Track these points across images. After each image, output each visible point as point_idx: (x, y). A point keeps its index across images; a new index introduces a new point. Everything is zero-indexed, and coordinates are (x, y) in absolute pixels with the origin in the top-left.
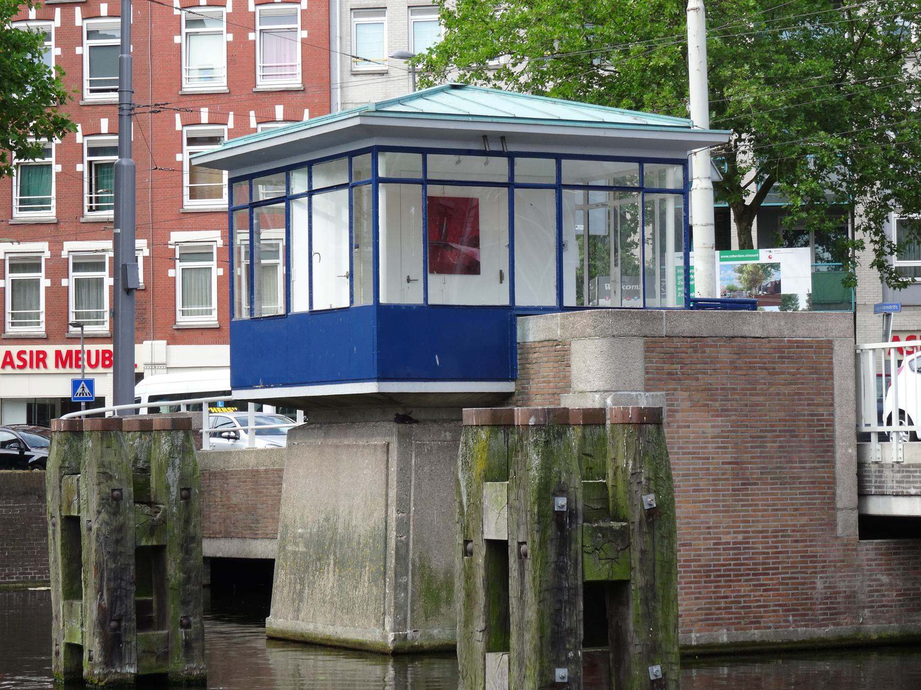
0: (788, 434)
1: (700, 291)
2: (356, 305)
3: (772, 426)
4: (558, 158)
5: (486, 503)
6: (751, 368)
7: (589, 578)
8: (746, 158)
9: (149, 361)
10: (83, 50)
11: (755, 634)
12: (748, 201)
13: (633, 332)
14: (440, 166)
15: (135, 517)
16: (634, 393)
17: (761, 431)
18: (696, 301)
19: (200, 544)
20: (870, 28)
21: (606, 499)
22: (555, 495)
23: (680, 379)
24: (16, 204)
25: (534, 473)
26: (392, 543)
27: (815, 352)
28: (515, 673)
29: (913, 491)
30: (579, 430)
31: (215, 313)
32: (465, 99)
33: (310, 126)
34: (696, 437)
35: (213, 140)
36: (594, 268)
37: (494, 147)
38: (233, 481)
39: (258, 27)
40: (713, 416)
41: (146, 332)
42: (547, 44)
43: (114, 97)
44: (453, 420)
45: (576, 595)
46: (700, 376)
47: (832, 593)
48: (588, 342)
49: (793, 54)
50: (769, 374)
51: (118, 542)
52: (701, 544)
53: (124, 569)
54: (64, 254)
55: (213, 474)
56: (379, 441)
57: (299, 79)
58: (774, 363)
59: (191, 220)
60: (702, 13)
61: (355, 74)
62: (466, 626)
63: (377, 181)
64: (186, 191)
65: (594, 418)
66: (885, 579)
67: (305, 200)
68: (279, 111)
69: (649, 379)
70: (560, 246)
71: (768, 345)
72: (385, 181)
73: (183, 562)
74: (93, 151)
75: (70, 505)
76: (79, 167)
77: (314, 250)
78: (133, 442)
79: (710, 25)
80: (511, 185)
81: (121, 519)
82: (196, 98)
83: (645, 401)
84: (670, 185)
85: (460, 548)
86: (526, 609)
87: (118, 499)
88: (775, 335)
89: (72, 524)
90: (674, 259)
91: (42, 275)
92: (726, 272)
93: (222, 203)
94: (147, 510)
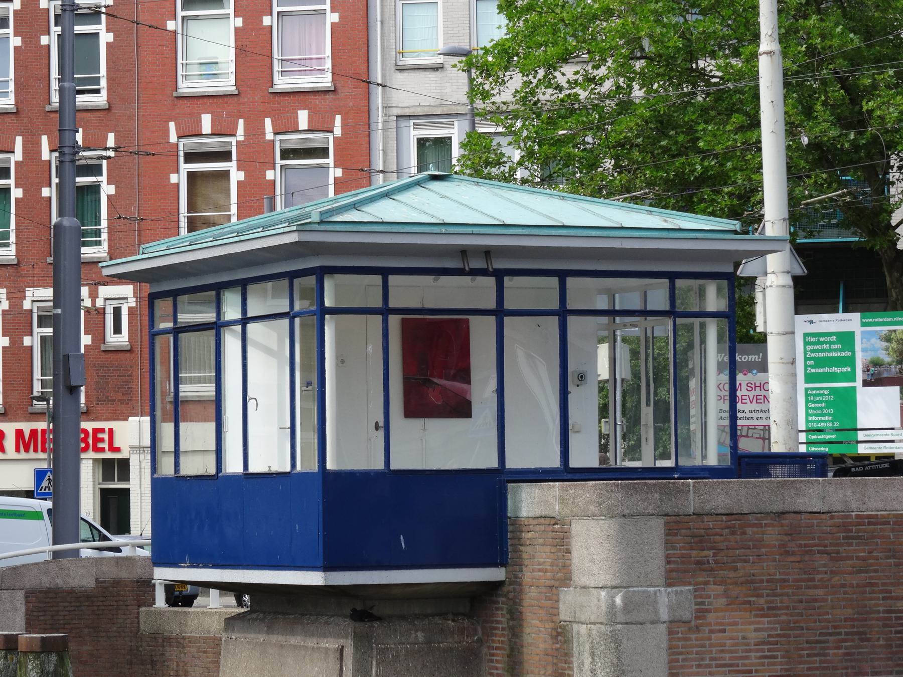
0: (856, 637)
3: (835, 627)
6: (807, 552)
9: (136, 443)
13: (650, 510)
16: (651, 589)
17: (821, 634)
23: (712, 570)
27: (893, 530)
32: (444, 197)
37: (477, 263)
40: (756, 616)
42: (634, 42)
44: (427, 616)
46: (739, 565)
48: (592, 523)
50: (832, 559)
54: (27, 305)
55: (168, 640)
56: (331, 644)
57: (329, 76)
58: (837, 545)
60: (778, 58)
61: (401, 69)
63: (324, 311)
64: (184, 224)
67: (239, 328)
69: (671, 571)
71: (830, 522)
72: (333, 311)
77: (250, 394)
82: (196, 101)
88: (839, 508)
92: (869, 340)
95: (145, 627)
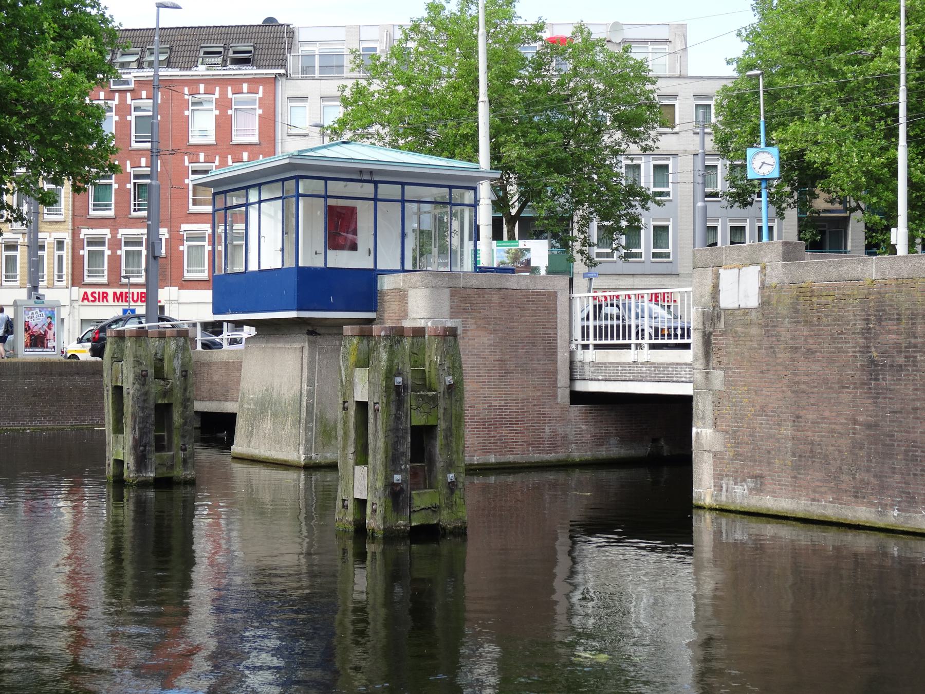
1: (483, 262)
2: (285, 266)
4: (403, 184)
5: (356, 380)
7: (413, 424)
8: (512, 189)
10: (131, 118)
11: (510, 458)
12: (514, 212)
14: (335, 188)
15: (155, 387)
18: (480, 268)
19: (192, 403)
20: (584, 116)
21: (425, 379)
22: (395, 376)
24: (91, 207)
25: (383, 363)
26: (304, 404)
28: (371, 477)
29: (600, 378)
30: (410, 339)
31: (206, 272)
33: (263, 163)
34: (477, 346)
35: (206, 172)
36: (422, 251)
38: (214, 368)
39: (234, 107)
41: (165, 281)
43: (148, 145)
45: (406, 433)
47: (554, 435)
48: (418, 290)
49: (540, 129)
51: (145, 401)
52: (481, 407)
53: (148, 416)
54: (119, 236)
56: (297, 345)
59: (193, 217)
61: (289, 135)
62: (344, 450)
63: (298, 195)
64: (191, 201)
65: (419, 333)
66: (584, 427)
67: (257, 205)
68: (245, 156)
70: (403, 236)
73: (183, 412)
74: (136, 177)
75: (117, 379)
76: (128, 186)
78: (154, 344)
79: (493, 111)
80: (375, 200)
81: (147, 388)
83: (449, 323)
84: (466, 202)
85: (341, 406)
86: (378, 441)
87: (145, 376)
89: (118, 391)
90: (469, 246)
91: (105, 248)
93: (209, 209)
94: (162, 382)
95: (194, 359)
